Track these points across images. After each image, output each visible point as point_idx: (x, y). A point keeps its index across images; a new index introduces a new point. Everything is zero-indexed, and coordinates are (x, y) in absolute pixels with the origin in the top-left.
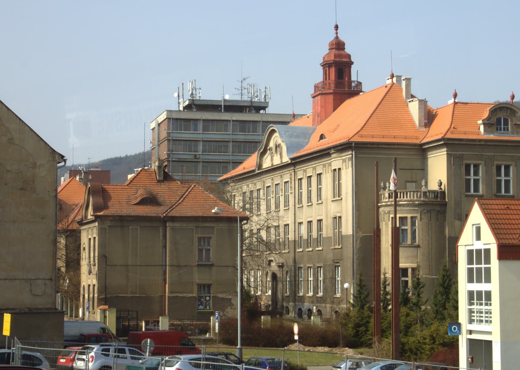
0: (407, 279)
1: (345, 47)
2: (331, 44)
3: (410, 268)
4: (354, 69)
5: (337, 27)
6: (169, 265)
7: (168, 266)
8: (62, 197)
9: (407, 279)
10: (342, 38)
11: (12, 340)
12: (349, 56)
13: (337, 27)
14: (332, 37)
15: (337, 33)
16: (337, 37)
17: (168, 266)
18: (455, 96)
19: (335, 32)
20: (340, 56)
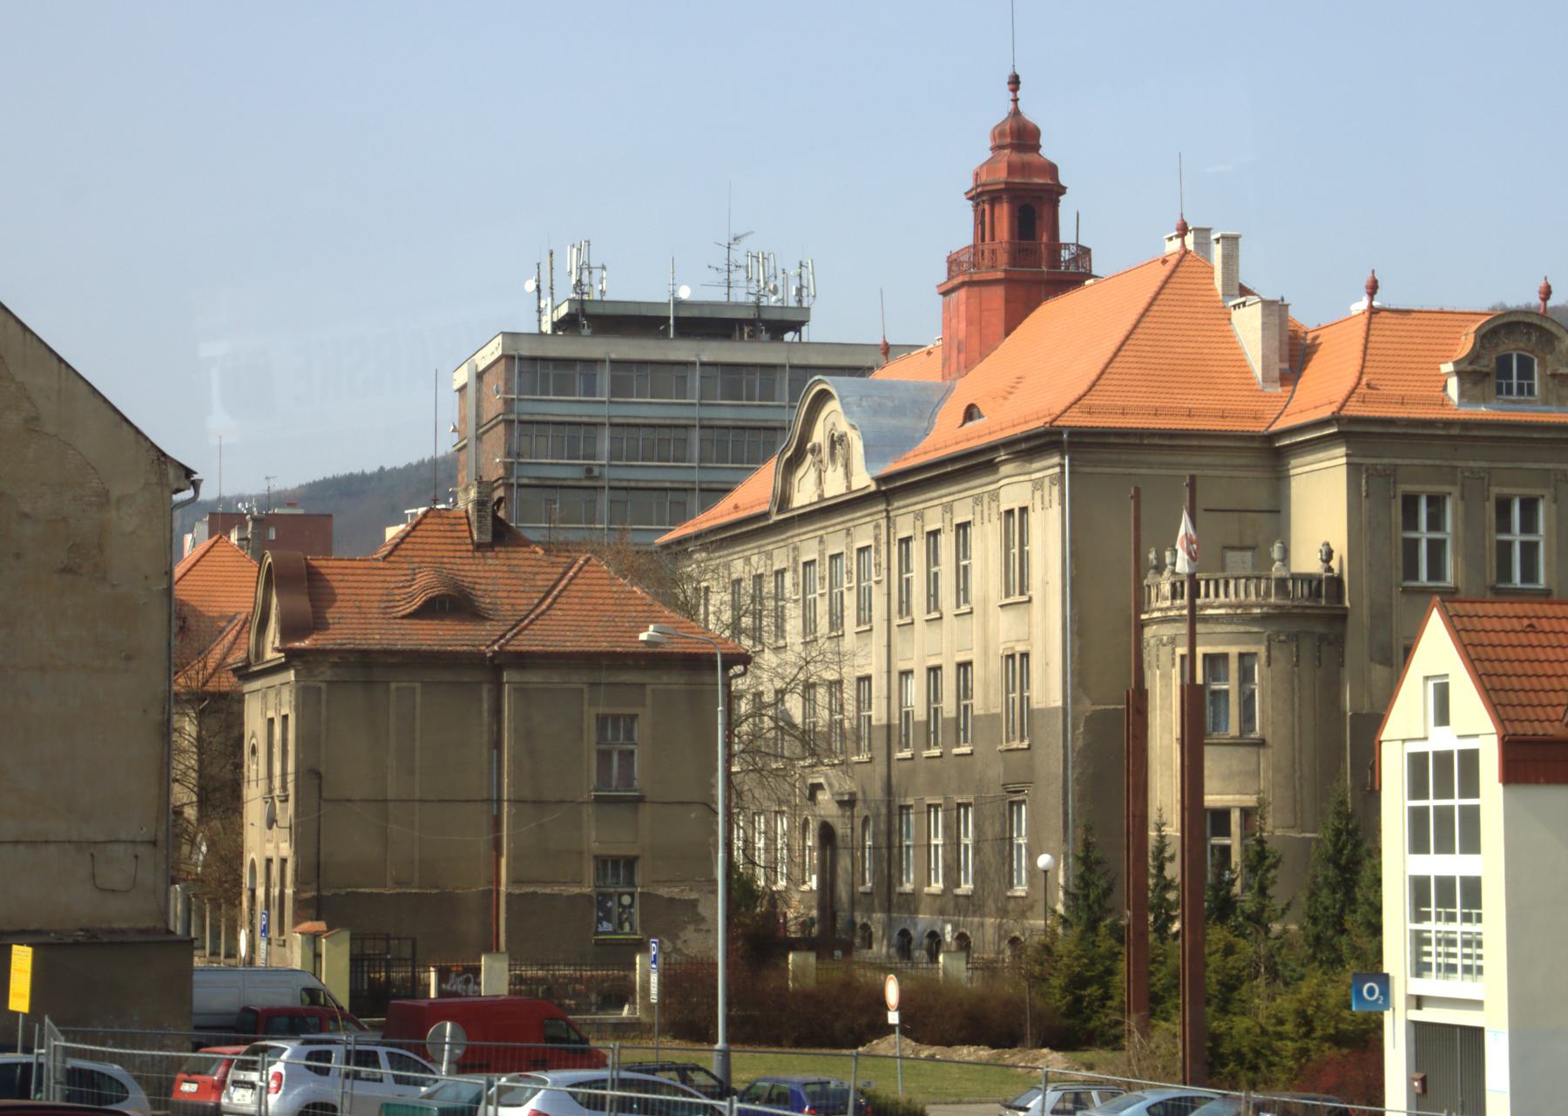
0: (1226, 841)
1: (1042, 142)
2: (998, 133)
3: (1235, 807)
4: (1067, 208)
5: (1015, 82)
6: (509, 801)
7: (506, 804)
8: (185, 593)
9: (1226, 841)
10: (1031, 114)
11: (37, 1026)
12: (1052, 170)
13: (1015, 82)
14: (1000, 112)
15: (1015, 100)
16: (1016, 113)
17: (506, 804)
18: (1373, 289)
19: (1011, 95)
20: (1025, 168)
